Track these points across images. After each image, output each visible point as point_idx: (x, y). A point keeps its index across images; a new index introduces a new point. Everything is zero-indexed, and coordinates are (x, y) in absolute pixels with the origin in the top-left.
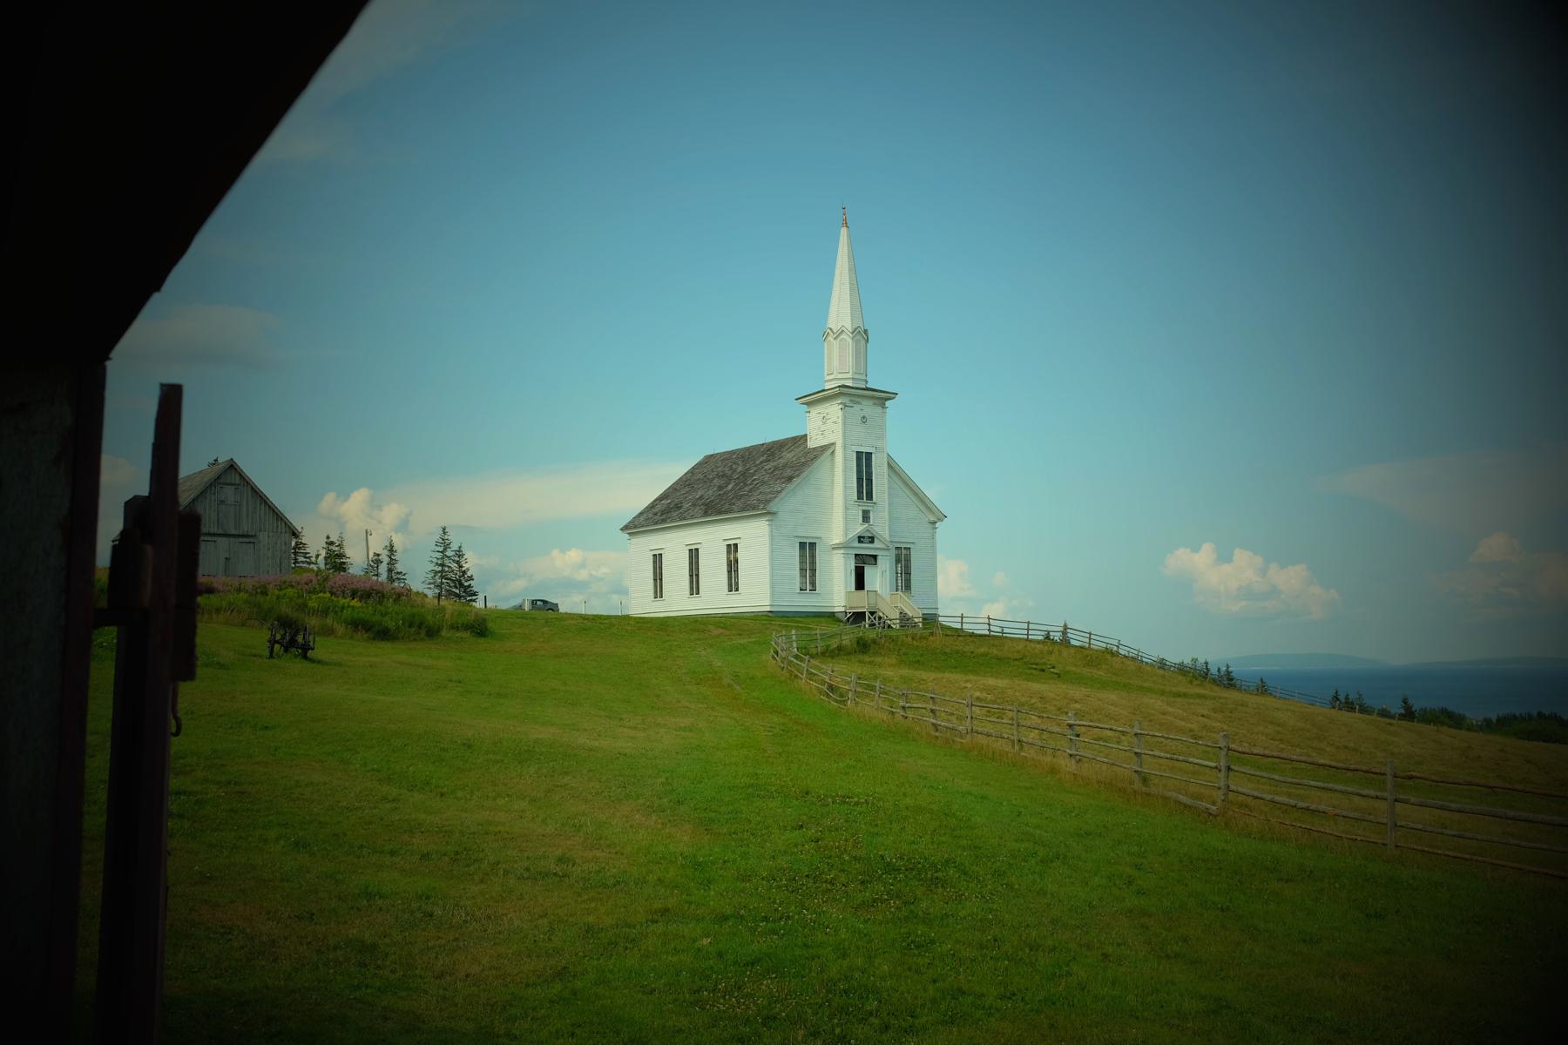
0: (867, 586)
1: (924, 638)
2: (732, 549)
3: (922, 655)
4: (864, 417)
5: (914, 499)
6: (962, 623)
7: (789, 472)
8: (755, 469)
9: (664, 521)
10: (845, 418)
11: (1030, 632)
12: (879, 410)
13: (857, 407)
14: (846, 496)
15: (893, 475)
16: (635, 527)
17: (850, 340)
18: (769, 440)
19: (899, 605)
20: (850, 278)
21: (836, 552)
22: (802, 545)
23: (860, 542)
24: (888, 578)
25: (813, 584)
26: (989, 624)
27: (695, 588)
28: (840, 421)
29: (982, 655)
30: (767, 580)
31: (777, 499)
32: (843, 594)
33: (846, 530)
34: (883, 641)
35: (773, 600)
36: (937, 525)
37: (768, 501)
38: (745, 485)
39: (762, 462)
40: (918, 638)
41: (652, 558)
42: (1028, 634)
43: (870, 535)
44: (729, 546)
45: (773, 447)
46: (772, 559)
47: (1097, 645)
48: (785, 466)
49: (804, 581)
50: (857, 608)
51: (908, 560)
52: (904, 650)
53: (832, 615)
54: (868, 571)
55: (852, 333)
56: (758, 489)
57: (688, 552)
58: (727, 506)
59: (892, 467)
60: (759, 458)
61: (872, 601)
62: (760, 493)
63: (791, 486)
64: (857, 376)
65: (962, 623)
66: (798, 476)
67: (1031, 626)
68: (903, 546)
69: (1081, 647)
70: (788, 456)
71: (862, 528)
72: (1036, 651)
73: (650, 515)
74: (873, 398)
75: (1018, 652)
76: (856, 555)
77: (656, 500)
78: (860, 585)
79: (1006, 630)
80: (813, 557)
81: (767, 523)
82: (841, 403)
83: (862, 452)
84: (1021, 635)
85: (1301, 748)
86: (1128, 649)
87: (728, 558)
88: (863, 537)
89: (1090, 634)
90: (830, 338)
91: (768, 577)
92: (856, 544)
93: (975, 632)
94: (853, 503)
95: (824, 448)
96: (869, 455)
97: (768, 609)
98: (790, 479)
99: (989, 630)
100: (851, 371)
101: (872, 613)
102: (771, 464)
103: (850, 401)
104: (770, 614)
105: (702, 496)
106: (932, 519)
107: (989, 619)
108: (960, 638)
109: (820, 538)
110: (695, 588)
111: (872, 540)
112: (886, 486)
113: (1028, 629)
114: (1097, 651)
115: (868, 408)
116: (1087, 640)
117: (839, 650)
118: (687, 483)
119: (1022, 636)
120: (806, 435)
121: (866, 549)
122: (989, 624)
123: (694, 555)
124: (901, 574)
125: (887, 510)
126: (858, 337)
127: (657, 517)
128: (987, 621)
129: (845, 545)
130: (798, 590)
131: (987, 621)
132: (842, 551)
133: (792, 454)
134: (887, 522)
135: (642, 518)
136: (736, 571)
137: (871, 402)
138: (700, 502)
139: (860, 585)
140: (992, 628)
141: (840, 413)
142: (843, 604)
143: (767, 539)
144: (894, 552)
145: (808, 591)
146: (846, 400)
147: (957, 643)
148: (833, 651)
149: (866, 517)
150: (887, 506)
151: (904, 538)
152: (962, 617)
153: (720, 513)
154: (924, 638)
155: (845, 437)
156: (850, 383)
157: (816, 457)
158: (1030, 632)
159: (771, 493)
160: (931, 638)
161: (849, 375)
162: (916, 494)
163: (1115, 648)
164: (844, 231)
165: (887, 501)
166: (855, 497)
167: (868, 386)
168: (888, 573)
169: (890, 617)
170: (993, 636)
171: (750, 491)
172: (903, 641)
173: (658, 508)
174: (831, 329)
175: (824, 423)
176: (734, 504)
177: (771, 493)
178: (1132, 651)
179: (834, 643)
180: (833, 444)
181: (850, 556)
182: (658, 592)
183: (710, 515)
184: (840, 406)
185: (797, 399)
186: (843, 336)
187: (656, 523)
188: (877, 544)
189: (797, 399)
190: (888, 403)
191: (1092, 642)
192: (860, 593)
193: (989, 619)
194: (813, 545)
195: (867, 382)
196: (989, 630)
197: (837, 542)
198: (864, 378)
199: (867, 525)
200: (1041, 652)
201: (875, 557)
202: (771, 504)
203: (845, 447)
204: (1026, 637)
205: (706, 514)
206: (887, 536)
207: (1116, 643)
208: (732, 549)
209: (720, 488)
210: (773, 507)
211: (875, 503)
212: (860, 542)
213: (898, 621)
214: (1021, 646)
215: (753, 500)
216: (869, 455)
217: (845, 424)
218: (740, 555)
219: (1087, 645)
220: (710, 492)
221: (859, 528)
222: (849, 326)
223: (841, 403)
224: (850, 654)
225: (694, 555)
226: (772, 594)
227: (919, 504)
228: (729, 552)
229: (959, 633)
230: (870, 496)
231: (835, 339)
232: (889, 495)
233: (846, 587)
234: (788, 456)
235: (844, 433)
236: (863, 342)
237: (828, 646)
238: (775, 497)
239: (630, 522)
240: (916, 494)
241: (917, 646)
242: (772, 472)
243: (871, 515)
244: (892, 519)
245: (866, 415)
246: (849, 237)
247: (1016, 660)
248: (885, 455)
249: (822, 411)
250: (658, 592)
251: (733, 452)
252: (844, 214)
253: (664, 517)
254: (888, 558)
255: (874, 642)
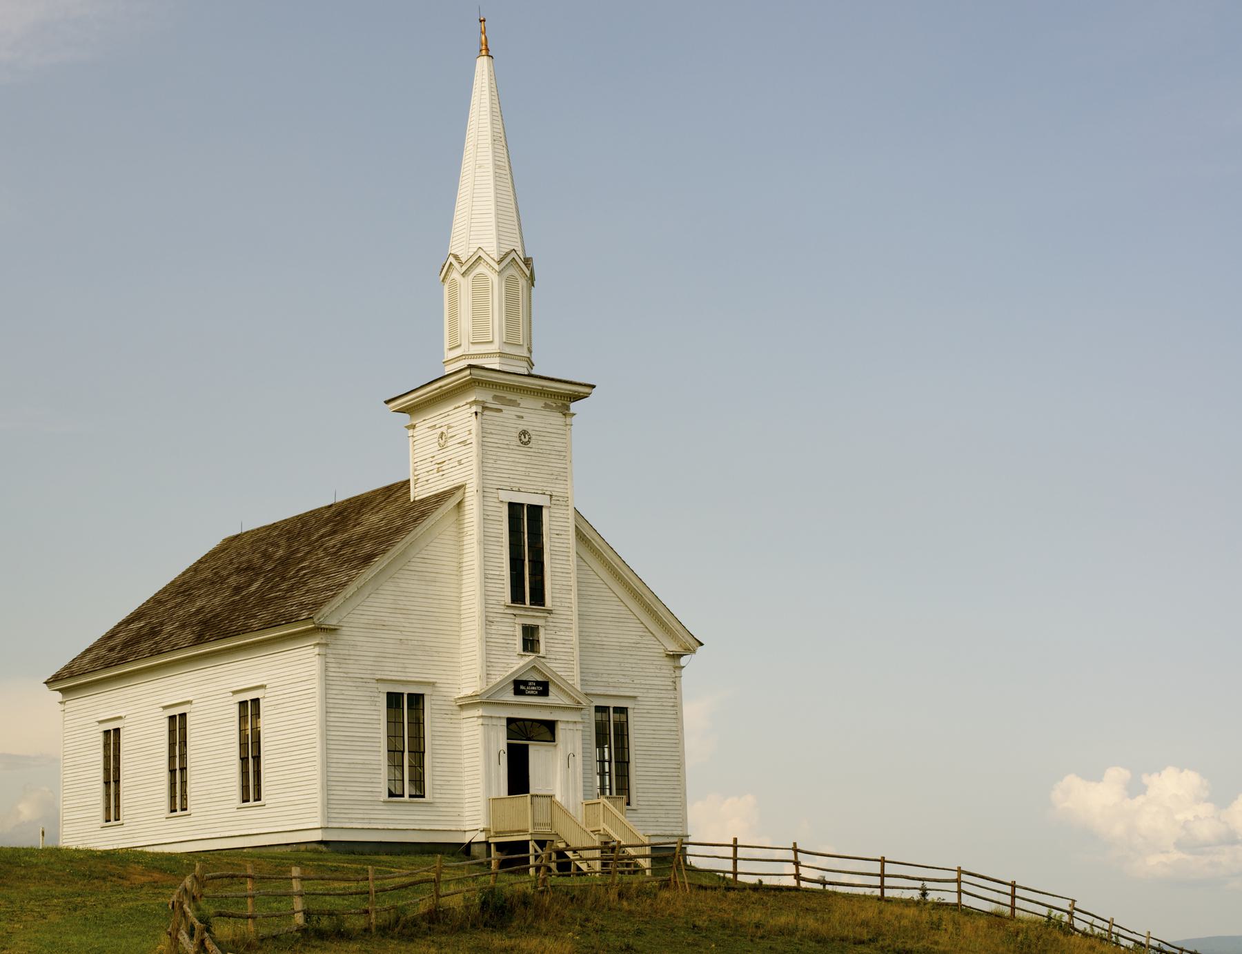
0: (536, 784)
1: (648, 894)
2: (250, 710)
3: (639, 933)
4: (524, 433)
5: (632, 605)
6: (735, 860)
7: (368, 547)
8: (307, 549)
9: (122, 660)
10: (484, 432)
11: (888, 882)
12: (556, 419)
13: (509, 412)
14: (486, 596)
15: (589, 557)
16: (72, 676)
17: (494, 278)
18: (342, 497)
19: (603, 826)
20: (492, 124)
21: (465, 714)
22: (394, 700)
23: (518, 692)
24: (579, 769)
25: (418, 782)
26: (797, 864)
27: (178, 799)
28: (473, 439)
29: (781, 932)
30: (315, 774)
31: (338, 600)
32: (481, 806)
33: (488, 665)
34: (547, 899)
35: (327, 816)
36: (683, 661)
37: (318, 605)
38: (284, 579)
39: (322, 537)
40: (633, 891)
41: (101, 738)
42: (882, 887)
43: (539, 679)
44: (243, 704)
45: (345, 510)
46: (327, 727)
47: (1029, 909)
48: (363, 537)
49: (399, 776)
50: (512, 832)
51: (622, 732)
52: (597, 919)
53: (464, 850)
54: (537, 755)
55: (499, 262)
56: (305, 584)
57: (167, 721)
58: (241, 621)
59: (585, 537)
60: (318, 530)
61: (543, 818)
62: (307, 591)
63: (369, 573)
64: (508, 350)
65: (735, 860)
66: (384, 551)
67: (889, 869)
68: (612, 703)
69: (998, 915)
70: (372, 520)
71: (522, 662)
72: (905, 922)
73: (103, 652)
74: (541, 393)
75: (865, 924)
76: (510, 721)
77: (120, 625)
78: (518, 781)
79: (830, 877)
80: (417, 724)
81: (317, 650)
82: (475, 402)
83: (522, 505)
84: (865, 886)
85: (376, 909)
86: (1089, 919)
87: (242, 731)
88: (526, 683)
89: (1013, 886)
90: (455, 275)
91: (318, 767)
92: (510, 697)
93: (767, 881)
94: (501, 609)
95: (441, 498)
96: (536, 511)
97: (317, 836)
98: (368, 559)
99: (797, 876)
100: (497, 340)
101: (542, 844)
102: (339, 538)
103: (495, 397)
104: (323, 848)
105: (203, 607)
106: (673, 647)
107: (796, 850)
108: (731, 894)
109: (433, 684)
110: (178, 799)
111: (543, 688)
112: (573, 576)
113: (882, 876)
114: (1028, 922)
115: (534, 416)
116: (1008, 900)
117: (431, 921)
118: (182, 589)
119: (868, 891)
120: (409, 481)
121: (531, 709)
122: (797, 864)
123: (178, 726)
124: (610, 762)
125: (575, 627)
126: (512, 271)
127: (114, 655)
128: (790, 855)
129: (484, 699)
130: (385, 796)
131: (790, 855)
132: (479, 712)
133: (381, 515)
134: (577, 653)
135: (86, 660)
136: (243, 745)
137: (539, 403)
138: (195, 620)
139: (518, 781)
140: (804, 872)
141: (474, 423)
142: (481, 827)
143: (316, 685)
144: (591, 717)
145: (406, 797)
146: (486, 396)
147: (725, 905)
148: (414, 923)
149: (530, 640)
150: (575, 617)
151: (612, 689)
152: (735, 846)
153: (226, 635)
154: (648, 894)
155: (483, 473)
156: (494, 363)
157: (424, 514)
158: (876, 881)
159: (326, 589)
160: (666, 894)
161: (494, 348)
162: (636, 596)
163: (1066, 918)
164: (483, 64)
165: (575, 608)
166: (507, 596)
167: (534, 372)
168: (579, 758)
169: (573, 845)
170: (806, 890)
171: (291, 589)
172: (597, 900)
173: (122, 637)
174: (456, 257)
175: (442, 447)
176: (254, 616)
177: (326, 589)
178: (1097, 922)
179: (421, 905)
180: (458, 488)
181: (495, 722)
182: (112, 810)
183: (207, 641)
184: (474, 409)
185: (387, 402)
186: (481, 269)
187: (108, 666)
188: (554, 698)
189: (387, 402)
190: (574, 407)
191: (1018, 903)
192: (522, 800)
193: (796, 850)
194: (417, 701)
195: (531, 365)
196: (797, 876)
197: (469, 692)
198: (526, 354)
199: (531, 657)
200: (917, 924)
201: (551, 726)
202: (325, 610)
203: (484, 492)
204: (877, 892)
205: (199, 640)
206: (576, 681)
207: (1065, 905)
208: (250, 710)
209: (237, 590)
210: (327, 615)
211: (550, 612)
212: (518, 692)
213: (597, 854)
214: (870, 913)
215: (291, 606)
216: (536, 511)
217: (483, 444)
218: (265, 723)
219: (1007, 910)
220: (217, 600)
221: (515, 663)
222: (492, 250)
223: (475, 402)
224: (461, 929)
225: (178, 726)
226: (328, 804)
227: (645, 618)
228: (243, 718)
229: (726, 886)
230: (538, 597)
231: (464, 274)
232: (580, 596)
233: (488, 787)
234: (372, 520)
235: (482, 462)
236: (522, 282)
237: (403, 910)
238: (333, 596)
239: (66, 668)
240: (636, 596)
241: (630, 912)
242: (335, 553)
243: (542, 636)
244: (586, 645)
245: (529, 429)
246: (498, 79)
247: (862, 942)
248: (571, 513)
249: (438, 422)
250: (112, 810)
251: (274, 526)
252: (483, 33)
253: (124, 653)
254: (580, 727)
255: (525, 901)
